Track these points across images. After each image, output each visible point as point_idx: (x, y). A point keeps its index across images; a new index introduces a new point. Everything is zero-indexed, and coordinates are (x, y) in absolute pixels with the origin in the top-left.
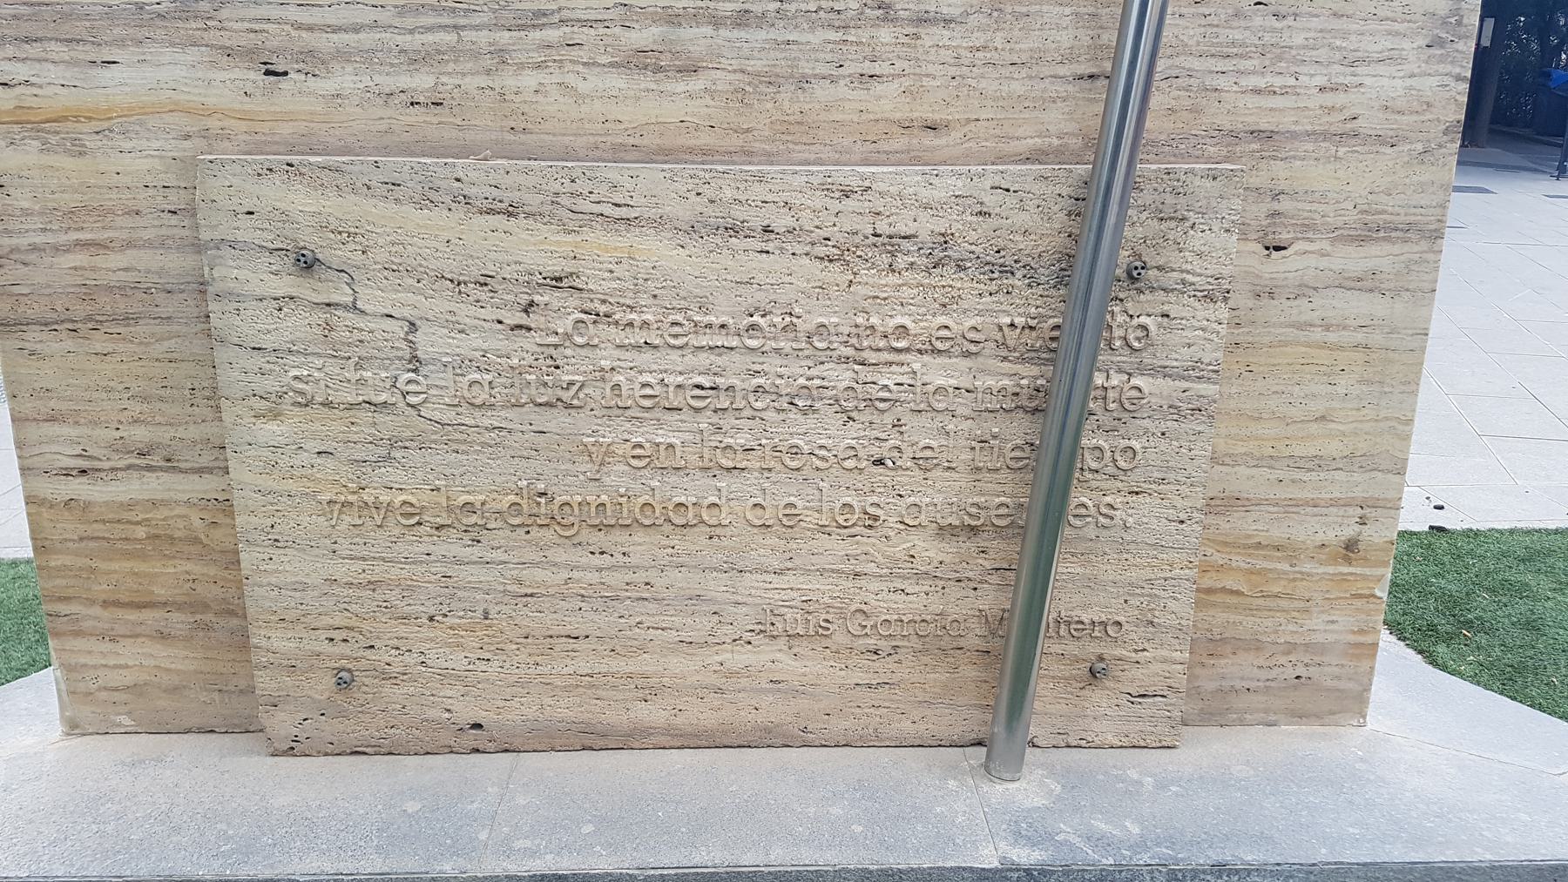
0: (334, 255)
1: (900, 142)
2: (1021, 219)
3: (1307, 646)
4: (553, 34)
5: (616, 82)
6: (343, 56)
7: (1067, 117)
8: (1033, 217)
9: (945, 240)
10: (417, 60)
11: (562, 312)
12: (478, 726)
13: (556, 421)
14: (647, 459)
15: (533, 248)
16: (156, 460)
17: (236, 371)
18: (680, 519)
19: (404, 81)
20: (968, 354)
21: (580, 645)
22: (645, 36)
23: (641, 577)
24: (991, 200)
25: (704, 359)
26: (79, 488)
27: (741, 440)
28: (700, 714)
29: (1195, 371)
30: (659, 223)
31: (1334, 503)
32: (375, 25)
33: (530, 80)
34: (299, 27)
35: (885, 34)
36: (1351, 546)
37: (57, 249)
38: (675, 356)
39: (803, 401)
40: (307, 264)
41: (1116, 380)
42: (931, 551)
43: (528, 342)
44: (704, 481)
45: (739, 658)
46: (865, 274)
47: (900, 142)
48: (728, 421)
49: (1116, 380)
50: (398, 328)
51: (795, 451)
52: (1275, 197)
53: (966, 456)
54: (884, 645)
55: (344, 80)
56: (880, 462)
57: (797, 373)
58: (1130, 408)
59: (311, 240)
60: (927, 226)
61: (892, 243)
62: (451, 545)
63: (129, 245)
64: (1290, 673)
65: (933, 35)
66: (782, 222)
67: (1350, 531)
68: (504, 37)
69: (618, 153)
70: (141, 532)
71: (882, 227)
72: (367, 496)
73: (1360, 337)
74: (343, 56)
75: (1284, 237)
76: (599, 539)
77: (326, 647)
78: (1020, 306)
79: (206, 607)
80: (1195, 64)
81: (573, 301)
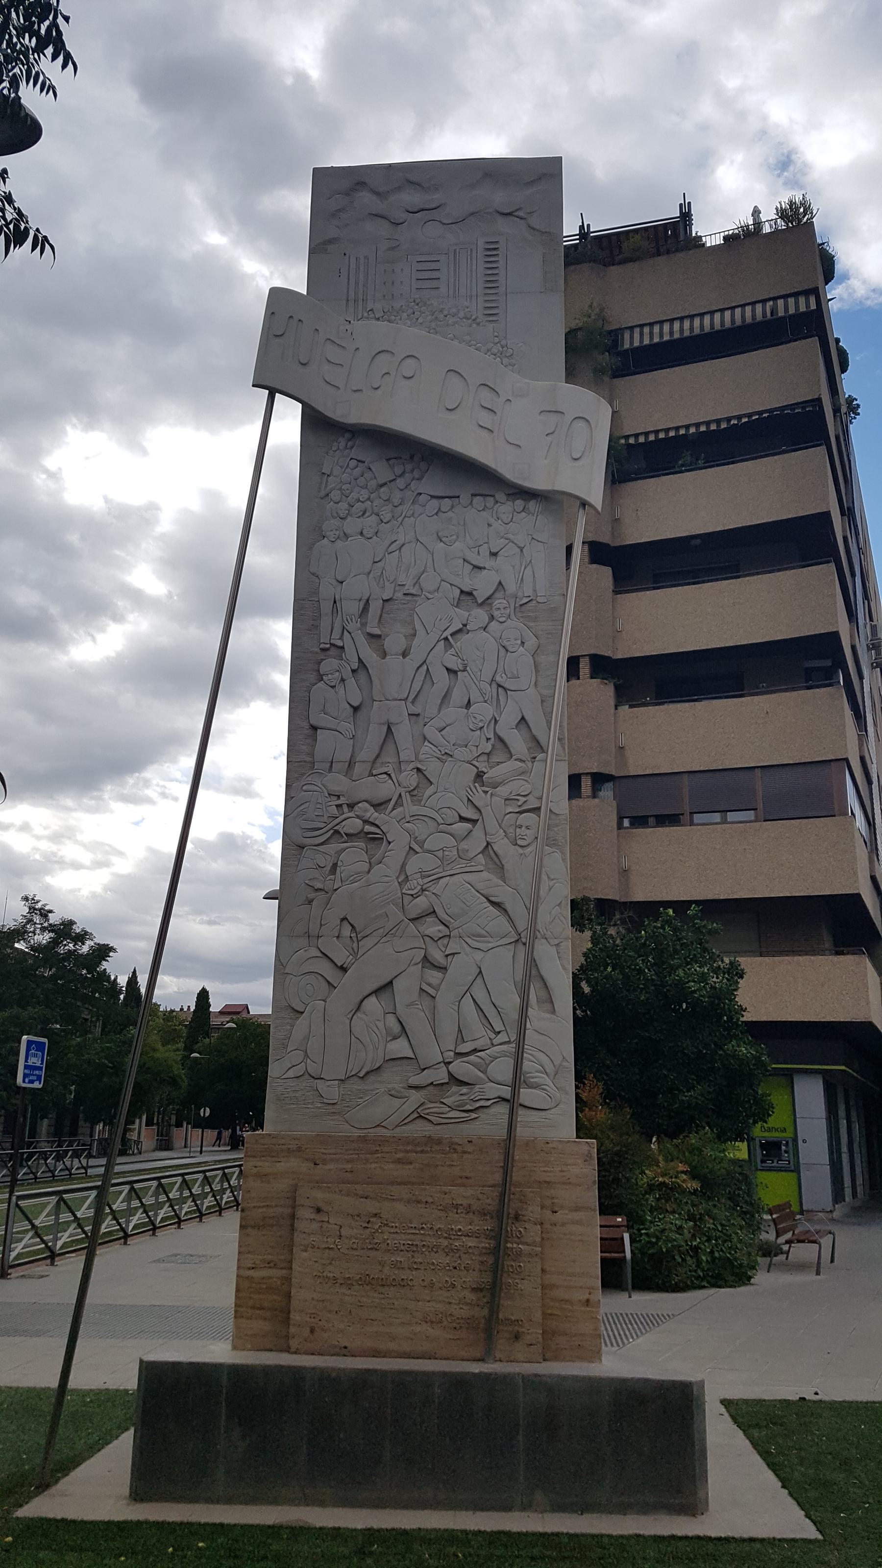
0: (325, 1208)
1: (459, 1181)
2: (489, 1201)
3: (581, 1334)
4: (379, 1155)
5: (392, 1166)
6: (332, 1160)
7: (498, 1177)
8: (490, 1201)
9: (470, 1205)
10: (348, 1161)
11: (376, 1223)
12: (346, 1348)
13: (373, 1254)
14: (396, 1265)
15: (370, 1206)
16: (272, 1264)
17: (298, 1238)
18: (402, 1284)
19: (344, 1166)
20: (477, 1237)
21: (376, 1323)
22: (399, 1155)
23: (391, 1301)
24: (480, 1196)
25: (410, 1237)
26: (251, 1273)
27: (420, 1260)
28: (406, 1347)
29: (534, 1244)
30: (400, 1200)
31: (581, 1287)
32: (341, 1153)
33: (373, 1166)
34: (323, 1153)
35: (455, 1155)
36: (588, 1301)
37: (259, 1207)
38: (403, 1236)
39: (434, 1249)
40: (319, 1210)
41: (515, 1245)
42: (470, 1296)
43: (368, 1231)
44: (408, 1272)
45: (418, 1329)
46: (451, 1214)
47: (459, 1181)
48: (416, 1255)
49: (515, 1245)
50: (337, 1228)
51: (433, 1264)
52: (553, 1198)
53: (478, 1266)
54: (458, 1326)
55: (331, 1166)
56: (455, 1268)
57: (433, 1241)
58: (520, 1254)
59: (320, 1204)
60: (465, 1202)
61: (457, 1206)
62: (344, 1290)
63: (276, 1206)
64: (577, 1343)
65: (466, 1156)
66: (430, 1200)
67: (587, 1296)
68: (368, 1156)
69: (392, 1183)
70: (264, 1286)
71: (454, 1202)
72: (325, 1274)
73: (580, 1238)
74: (332, 1160)
75: (557, 1209)
76: (381, 1289)
77: (308, 1319)
78: (489, 1225)
79: (276, 1310)
80: (529, 1164)
81: (379, 1220)
